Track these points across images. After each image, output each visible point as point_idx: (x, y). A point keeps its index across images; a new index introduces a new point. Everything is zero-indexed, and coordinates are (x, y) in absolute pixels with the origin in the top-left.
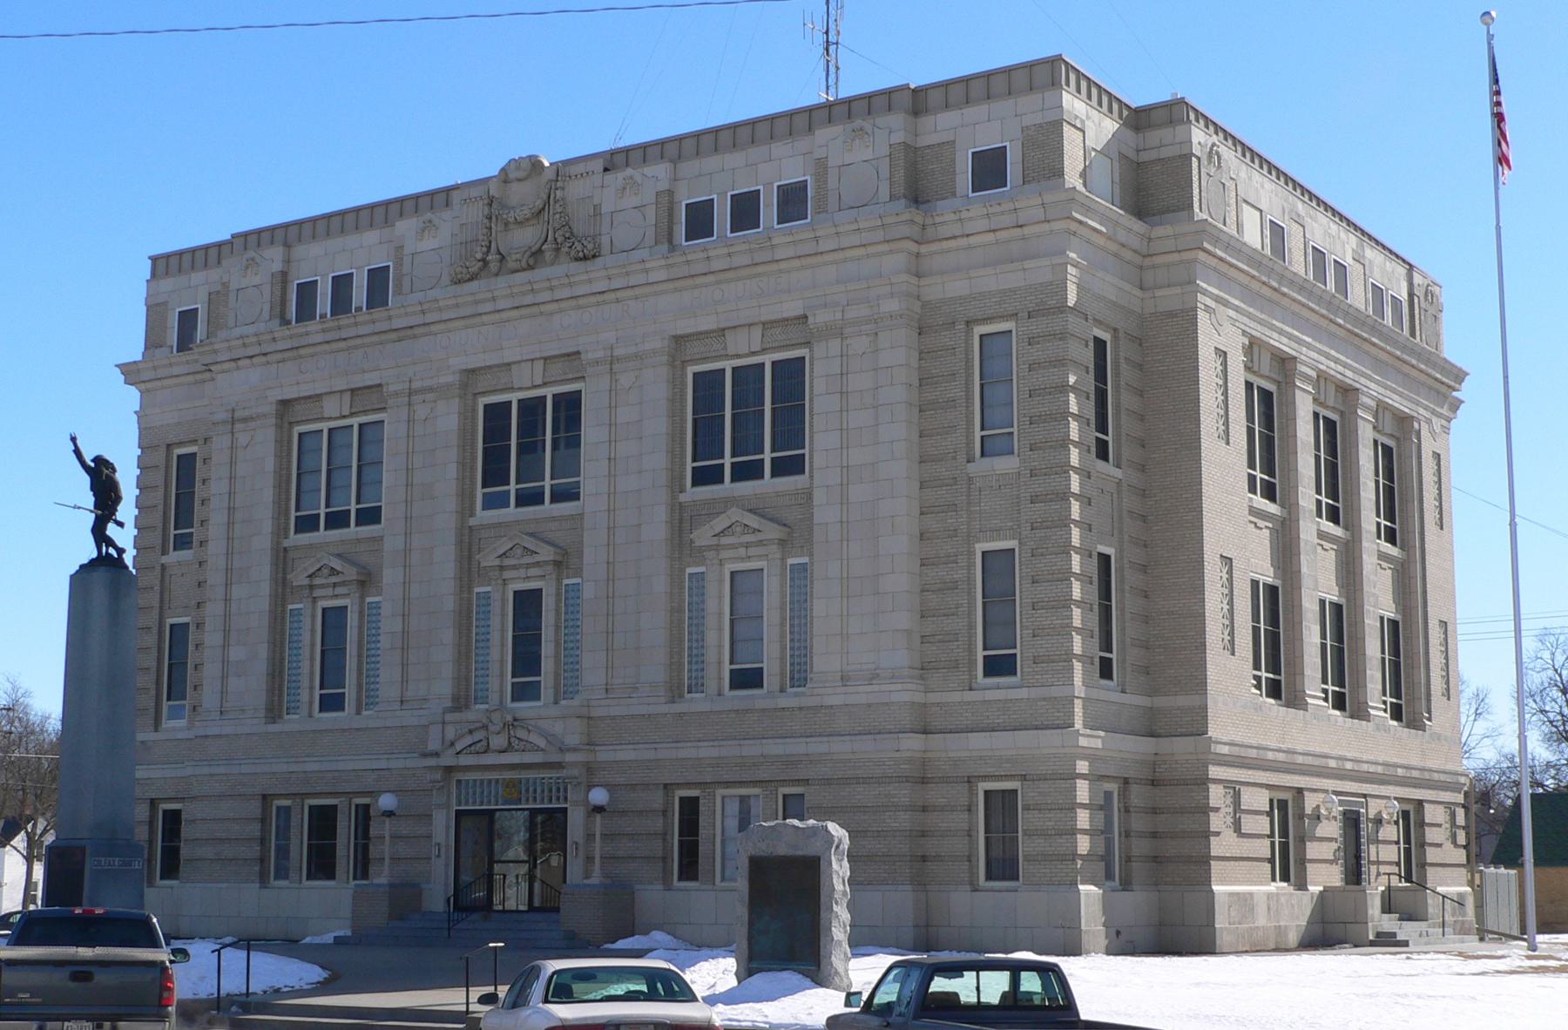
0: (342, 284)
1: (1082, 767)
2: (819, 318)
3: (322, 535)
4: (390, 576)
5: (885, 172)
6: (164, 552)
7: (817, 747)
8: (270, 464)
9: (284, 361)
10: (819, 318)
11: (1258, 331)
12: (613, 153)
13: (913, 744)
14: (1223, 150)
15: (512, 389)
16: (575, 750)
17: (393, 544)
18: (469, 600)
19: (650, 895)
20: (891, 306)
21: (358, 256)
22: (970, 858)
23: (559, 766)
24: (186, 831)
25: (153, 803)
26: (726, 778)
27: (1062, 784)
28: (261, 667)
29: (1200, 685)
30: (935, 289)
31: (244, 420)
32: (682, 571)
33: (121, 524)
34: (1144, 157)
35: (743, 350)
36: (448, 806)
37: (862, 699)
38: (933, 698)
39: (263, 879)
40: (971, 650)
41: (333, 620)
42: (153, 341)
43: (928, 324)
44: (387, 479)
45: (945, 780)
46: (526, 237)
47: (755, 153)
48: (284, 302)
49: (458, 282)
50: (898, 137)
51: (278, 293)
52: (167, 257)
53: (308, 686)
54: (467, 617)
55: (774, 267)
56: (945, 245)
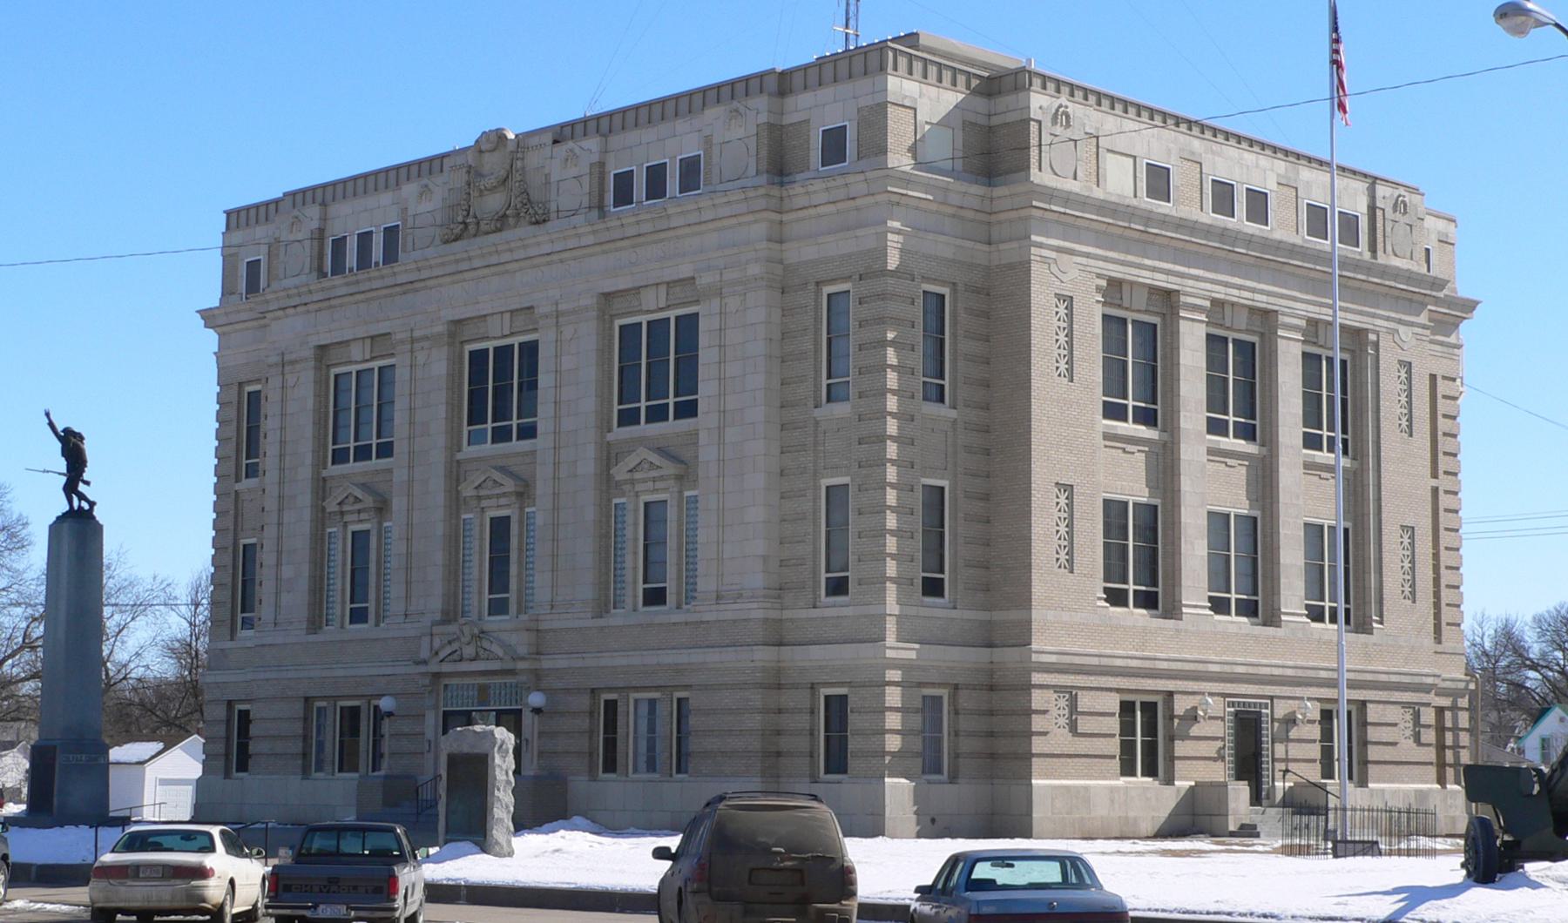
0: (365, 239)
1: (894, 675)
2: (705, 280)
3: (352, 467)
4: (398, 503)
5: (753, 151)
6: (238, 480)
7: (697, 657)
8: (310, 403)
9: (320, 310)
10: (705, 280)
11: (1117, 271)
12: (563, 126)
13: (764, 656)
14: (1072, 108)
15: (487, 338)
16: (523, 659)
17: (400, 475)
18: (457, 525)
19: (579, 785)
20: (755, 270)
21: (375, 215)
22: (812, 755)
23: (512, 672)
24: (254, 730)
25: (230, 704)
26: (634, 683)
27: (877, 690)
28: (303, 584)
29: (1025, 602)
30: (801, 253)
31: (293, 362)
32: (609, 500)
33: (87, 483)
34: (995, 121)
35: (651, 308)
36: (436, 707)
37: (729, 616)
38: (787, 614)
39: (305, 772)
40: (815, 573)
41: (360, 539)
42: (227, 291)
43: (786, 284)
44: (397, 415)
45: (795, 686)
46: (494, 202)
47: (664, 128)
48: (321, 256)
49: (446, 242)
50: (763, 118)
51: (316, 249)
52: (238, 211)
53: (340, 605)
54: (455, 540)
55: (671, 233)
56: (801, 214)
